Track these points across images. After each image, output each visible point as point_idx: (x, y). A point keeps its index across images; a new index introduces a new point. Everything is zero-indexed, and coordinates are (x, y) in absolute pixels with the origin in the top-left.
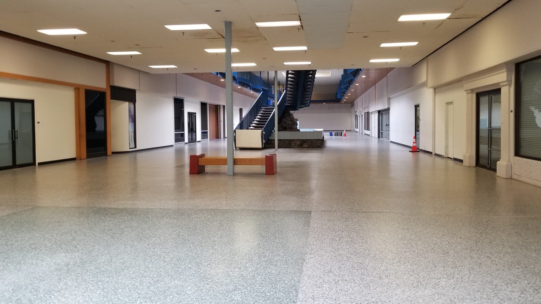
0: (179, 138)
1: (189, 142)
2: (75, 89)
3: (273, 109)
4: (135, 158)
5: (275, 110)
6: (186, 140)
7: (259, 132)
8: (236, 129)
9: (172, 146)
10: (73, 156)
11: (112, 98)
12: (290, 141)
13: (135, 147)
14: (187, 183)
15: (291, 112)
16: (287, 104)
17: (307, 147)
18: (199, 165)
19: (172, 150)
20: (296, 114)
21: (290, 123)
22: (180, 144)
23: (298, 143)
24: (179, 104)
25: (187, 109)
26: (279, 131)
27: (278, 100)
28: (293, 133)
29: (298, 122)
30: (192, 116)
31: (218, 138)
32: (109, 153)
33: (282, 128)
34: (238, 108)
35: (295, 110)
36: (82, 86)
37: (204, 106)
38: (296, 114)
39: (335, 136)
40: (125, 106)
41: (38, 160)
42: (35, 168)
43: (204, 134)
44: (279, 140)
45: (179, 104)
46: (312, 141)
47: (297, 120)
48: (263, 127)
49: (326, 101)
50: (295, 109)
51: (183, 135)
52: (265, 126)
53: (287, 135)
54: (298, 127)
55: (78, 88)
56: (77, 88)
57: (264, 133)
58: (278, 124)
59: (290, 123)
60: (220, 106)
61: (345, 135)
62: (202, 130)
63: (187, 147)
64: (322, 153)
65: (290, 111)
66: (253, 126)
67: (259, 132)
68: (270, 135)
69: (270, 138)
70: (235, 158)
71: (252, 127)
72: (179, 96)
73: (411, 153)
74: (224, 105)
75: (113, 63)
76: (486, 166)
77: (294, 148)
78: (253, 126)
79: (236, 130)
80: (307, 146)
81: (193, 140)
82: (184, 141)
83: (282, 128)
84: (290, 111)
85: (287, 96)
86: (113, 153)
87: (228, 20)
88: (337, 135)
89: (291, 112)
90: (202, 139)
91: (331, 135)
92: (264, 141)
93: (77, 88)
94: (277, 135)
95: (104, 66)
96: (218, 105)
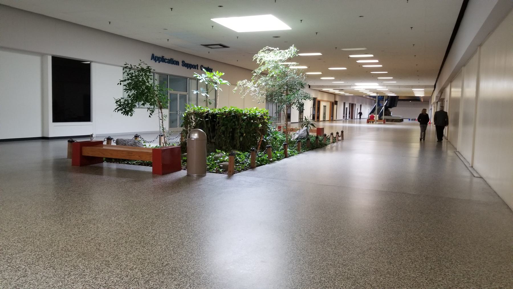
0: (344, 117)
1: (345, 119)
3: (383, 106)
10: (329, 120)
13: (336, 119)
17: (110, 160)
18: (83, 155)
20: (390, 109)
21: (388, 113)
23: (391, 120)
24: (344, 104)
25: (346, 107)
28: (389, 116)
29: (391, 113)
30: (347, 108)
33: (385, 115)
34: (360, 105)
37: (350, 104)
38: (390, 109)
40: (336, 105)
41: (326, 120)
45: (344, 104)
47: (391, 112)
50: (391, 108)
54: (391, 115)
56: (330, 102)
64: (323, 150)
75: (336, 94)
76: (207, 71)
83: (385, 115)
93: (330, 102)
95: (334, 95)
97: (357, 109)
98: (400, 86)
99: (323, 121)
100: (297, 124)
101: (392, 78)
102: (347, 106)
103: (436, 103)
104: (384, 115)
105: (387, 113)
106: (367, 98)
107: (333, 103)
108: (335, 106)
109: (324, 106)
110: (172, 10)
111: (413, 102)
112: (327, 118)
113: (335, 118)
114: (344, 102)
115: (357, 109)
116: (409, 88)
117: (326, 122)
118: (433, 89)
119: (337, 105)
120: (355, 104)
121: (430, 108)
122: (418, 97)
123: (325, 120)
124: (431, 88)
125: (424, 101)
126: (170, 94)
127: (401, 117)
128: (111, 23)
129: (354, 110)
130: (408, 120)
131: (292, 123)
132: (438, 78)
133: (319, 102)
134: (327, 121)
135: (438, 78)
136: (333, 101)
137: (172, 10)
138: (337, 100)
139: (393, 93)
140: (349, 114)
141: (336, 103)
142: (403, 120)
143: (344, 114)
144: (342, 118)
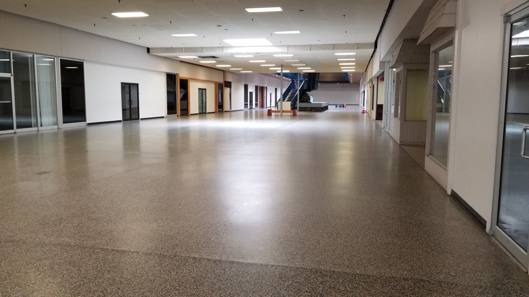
0: (246, 105)
1: (250, 109)
2: (215, 83)
3: (297, 91)
4: (231, 114)
5: (298, 92)
6: (249, 108)
7: (290, 103)
8: (278, 101)
9: (243, 110)
10: (214, 111)
11: (225, 87)
12: (306, 108)
13: (231, 109)
14: (267, 118)
15: (307, 92)
16: (305, 88)
19: (243, 112)
21: (306, 98)
22: (246, 109)
23: (309, 109)
24: (246, 87)
25: (250, 90)
26: (299, 102)
27: (299, 87)
28: (307, 104)
30: (251, 93)
31: (263, 107)
32: (189, 114)
35: (309, 91)
36: (218, 82)
37: (256, 87)
39: (339, 107)
40: (228, 89)
41: (140, 117)
42: (206, 115)
43: (256, 104)
44: (299, 107)
45: (246, 87)
46: (316, 108)
48: (291, 101)
49: (340, 82)
50: (309, 91)
51: (247, 104)
52: (292, 100)
53: (304, 105)
55: (216, 83)
56: (216, 83)
57: (292, 103)
58: (299, 99)
59: (306, 98)
60: (264, 87)
61: (345, 107)
62: (245, 102)
63: (249, 111)
65: (307, 92)
66: (286, 100)
67: (290, 103)
68: (295, 105)
69: (295, 106)
70: (283, 110)
71: (286, 101)
72: (247, 83)
73: (362, 114)
74: (267, 86)
75: (226, 71)
77: (307, 111)
78: (286, 100)
79: (278, 102)
80: (314, 110)
81: (251, 108)
82: (248, 108)
83: (301, 101)
84: (307, 92)
85: (305, 85)
86: (225, 111)
87: (282, 64)
88: (340, 107)
89: (307, 92)
90: (245, 108)
91: (336, 107)
92: (292, 108)
93: (216, 83)
94: (298, 105)
96: (263, 87)
97: (271, 94)
98: (311, 47)
99: (200, 113)
100: (120, 125)
101: (279, 9)
102: (251, 89)
103: (376, 79)
104: (300, 102)
105: (304, 98)
106: (276, 77)
107: (223, 85)
108: (227, 91)
109: (199, 89)
110: (119, 2)
111: (341, 85)
112: (211, 106)
113: (226, 107)
114: (245, 83)
115: (271, 94)
116: (329, 49)
117: (207, 115)
118: (373, 49)
119: (230, 87)
120: (266, 87)
121: (362, 90)
122: (346, 74)
123: (204, 111)
124: (368, 48)
125: (353, 83)
126: (250, 92)
127: (324, 103)
128: (27, 6)
129: (265, 96)
130: (335, 106)
131: (89, 124)
132: (386, 16)
133: (184, 84)
134: (208, 113)
135: (386, 16)
136: (221, 81)
137: (119, 2)
138: (229, 79)
139: (307, 66)
140: (256, 100)
141: (228, 85)
142: (328, 107)
143: (246, 100)
144: (242, 107)
